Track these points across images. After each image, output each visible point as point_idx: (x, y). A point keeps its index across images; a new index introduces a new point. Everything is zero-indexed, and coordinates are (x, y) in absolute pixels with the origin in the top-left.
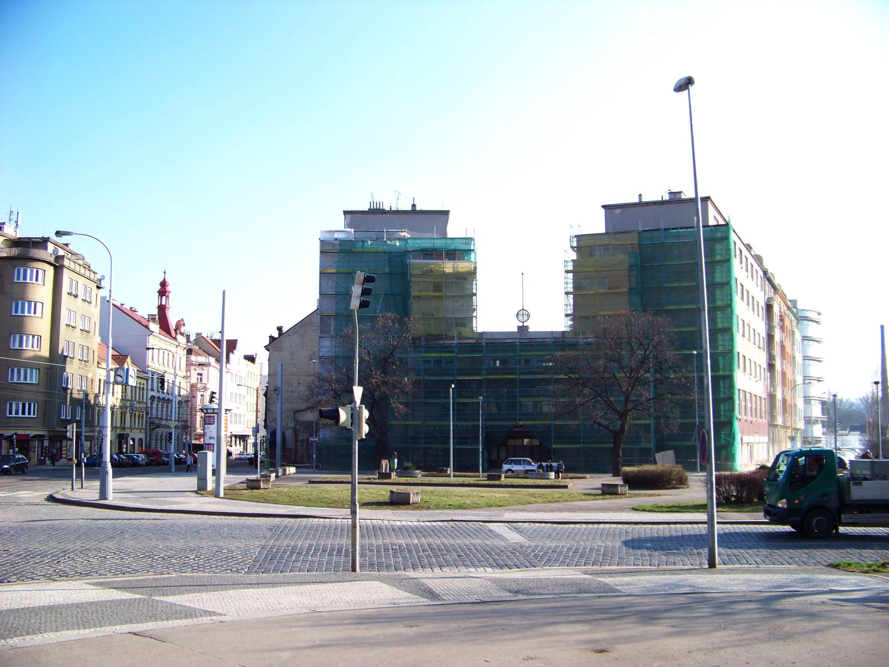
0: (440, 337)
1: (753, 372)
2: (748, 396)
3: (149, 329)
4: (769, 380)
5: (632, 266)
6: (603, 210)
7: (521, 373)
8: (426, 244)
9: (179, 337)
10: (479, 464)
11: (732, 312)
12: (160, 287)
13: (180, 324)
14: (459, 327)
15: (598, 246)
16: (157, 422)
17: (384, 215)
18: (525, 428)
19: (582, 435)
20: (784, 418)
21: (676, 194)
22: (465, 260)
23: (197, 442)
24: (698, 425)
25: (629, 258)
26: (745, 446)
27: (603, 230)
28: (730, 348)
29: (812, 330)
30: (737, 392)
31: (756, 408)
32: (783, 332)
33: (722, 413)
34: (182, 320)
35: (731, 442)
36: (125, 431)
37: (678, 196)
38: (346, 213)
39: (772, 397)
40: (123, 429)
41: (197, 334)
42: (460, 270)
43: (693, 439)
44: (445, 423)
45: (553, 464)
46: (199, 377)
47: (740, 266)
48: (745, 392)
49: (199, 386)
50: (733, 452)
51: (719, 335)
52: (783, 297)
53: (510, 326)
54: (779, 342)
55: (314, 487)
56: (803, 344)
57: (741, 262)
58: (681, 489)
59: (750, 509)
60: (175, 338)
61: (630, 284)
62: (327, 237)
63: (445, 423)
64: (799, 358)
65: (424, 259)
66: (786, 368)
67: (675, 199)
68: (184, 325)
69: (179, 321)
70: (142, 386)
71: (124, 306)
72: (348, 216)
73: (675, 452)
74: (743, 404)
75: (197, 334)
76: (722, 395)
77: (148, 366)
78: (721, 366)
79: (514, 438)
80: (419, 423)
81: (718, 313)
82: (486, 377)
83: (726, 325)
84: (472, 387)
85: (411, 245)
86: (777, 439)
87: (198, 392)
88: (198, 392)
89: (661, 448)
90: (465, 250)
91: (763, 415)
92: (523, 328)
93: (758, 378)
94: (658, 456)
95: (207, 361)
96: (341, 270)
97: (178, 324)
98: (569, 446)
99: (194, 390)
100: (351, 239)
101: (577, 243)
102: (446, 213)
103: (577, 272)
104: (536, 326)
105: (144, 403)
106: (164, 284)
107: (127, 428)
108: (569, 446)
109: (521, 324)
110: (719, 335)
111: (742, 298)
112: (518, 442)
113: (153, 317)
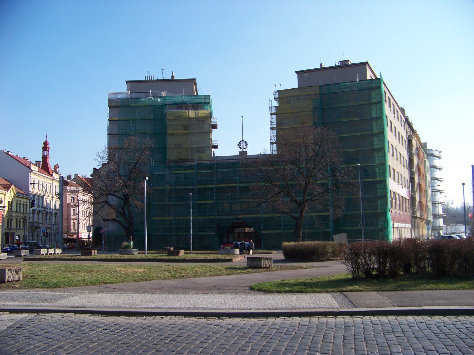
0: (186, 160)
1: (400, 181)
2: (397, 196)
3: (30, 169)
4: (410, 187)
5: (315, 108)
6: (296, 75)
7: (240, 183)
8: (179, 99)
9: (55, 175)
10: (190, 243)
11: (384, 137)
12: (43, 145)
13: (56, 167)
14: (199, 153)
15: (292, 97)
16: (36, 225)
17: (153, 83)
18: (243, 220)
19: (282, 224)
20: (420, 212)
21: (345, 62)
22: (204, 109)
23: (72, 237)
24: (362, 215)
25: (313, 103)
26: (395, 230)
27: (296, 86)
28: (384, 162)
29: (437, 162)
30: (389, 192)
31: (403, 205)
32: (419, 159)
33: (379, 206)
34: (58, 164)
35: (386, 226)
36: (11, 231)
37: (346, 63)
38: (127, 82)
39: (413, 199)
40: (10, 229)
41: (75, 175)
42: (200, 115)
43: (360, 225)
44: (188, 218)
45: (245, 243)
46: (72, 199)
47: (389, 108)
48: (395, 193)
49: (72, 205)
50: (387, 233)
51: (376, 153)
52: (418, 139)
53: (234, 151)
54: (416, 164)
55: (54, 263)
56: (430, 170)
57: (390, 107)
58: (334, 261)
59: (393, 285)
60: (52, 175)
61: (314, 120)
62: (113, 97)
63: (188, 218)
64: (429, 178)
65: (177, 109)
66: (421, 181)
67: (345, 65)
68: (58, 167)
69: (55, 166)
70: (25, 203)
71: (18, 156)
72: (129, 85)
73: (348, 235)
74: (394, 201)
75: (75, 175)
76: (379, 194)
77: (30, 191)
78: (378, 174)
79: (239, 227)
80: (171, 218)
81: (375, 138)
82: (216, 186)
83: (381, 146)
84: (208, 193)
85: (168, 101)
86: (417, 226)
87: (72, 208)
88: (72, 208)
89: (338, 231)
90: (204, 103)
91: (408, 210)
92: (243, 153)
93: (403, 185)
94: (335, 237)
95: (77, 190)
96: (121, 119)
97: (55, 167)
98: (274, 232)
99: (69, 207)
100: (128, 98)
101: (279, 96)
102: (194, 80)
103: (278, 114)
104: (252, 151)
105: (27, 214)
106: (46, 143)
107: (13, 229)
108: (274, 232)
109: (242, 150)
110: (376, 153)
111: (391, 131)
112: (241, 230)
113: (39, 163)
